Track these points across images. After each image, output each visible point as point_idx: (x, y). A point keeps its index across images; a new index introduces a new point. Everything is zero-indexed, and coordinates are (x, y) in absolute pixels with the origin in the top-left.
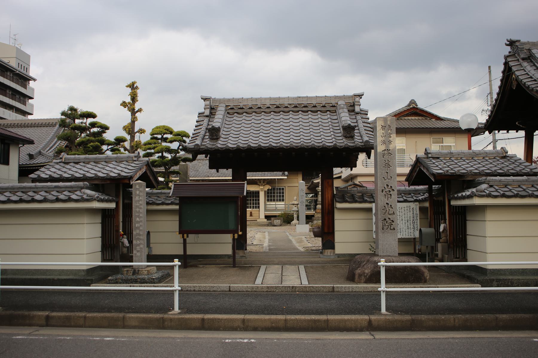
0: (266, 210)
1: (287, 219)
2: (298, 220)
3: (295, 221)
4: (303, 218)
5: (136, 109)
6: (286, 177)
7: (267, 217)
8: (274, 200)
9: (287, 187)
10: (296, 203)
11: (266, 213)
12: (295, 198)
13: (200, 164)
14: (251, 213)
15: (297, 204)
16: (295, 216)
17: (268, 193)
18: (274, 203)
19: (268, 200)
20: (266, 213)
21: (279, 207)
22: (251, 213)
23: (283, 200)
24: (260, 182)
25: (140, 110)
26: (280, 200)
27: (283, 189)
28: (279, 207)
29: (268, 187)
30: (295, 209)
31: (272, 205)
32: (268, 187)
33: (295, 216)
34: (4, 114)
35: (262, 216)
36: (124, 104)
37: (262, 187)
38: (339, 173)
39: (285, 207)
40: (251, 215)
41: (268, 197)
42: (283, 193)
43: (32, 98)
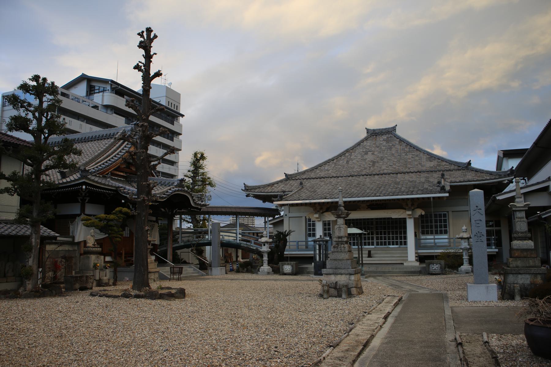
0: (418, 245)
1: (452, 263)
2: (471, 262)
3: (466, 267)
4: (481, 260)
5: (152, 73)
6: (447, 195)
7: (421, 259)
8: (432, 233)
9: (450, 213)
10: (465, 235)
11: (419, 251)
12: (464, 228)
13: (323, 183)
14: (369, 252)
15: (468, 239)
16: (465, 257)
17: (422, 222)
18: (432, 237)
19: (423, 233)
20: (419, 251)
21: (439, 242)
22: (369, 252)
23: (446, 232)
24: (407, 205)
25: (158, 74)
26: (441, 233)
27: (445, 216)
28: (439, 242)
29: (419, 212)
30: (465, 245)
31: (429, 239)
32: (419, 212)
33: (465, 257)
34: (157, 152)
35: (411, 255)
36: (137, 67)
37: (410, 213)
38: (543, 182)
39: (450, 242)
40: (370, 256)
41: (423, 227)
42: (445, 221)
43: (181, 134)
